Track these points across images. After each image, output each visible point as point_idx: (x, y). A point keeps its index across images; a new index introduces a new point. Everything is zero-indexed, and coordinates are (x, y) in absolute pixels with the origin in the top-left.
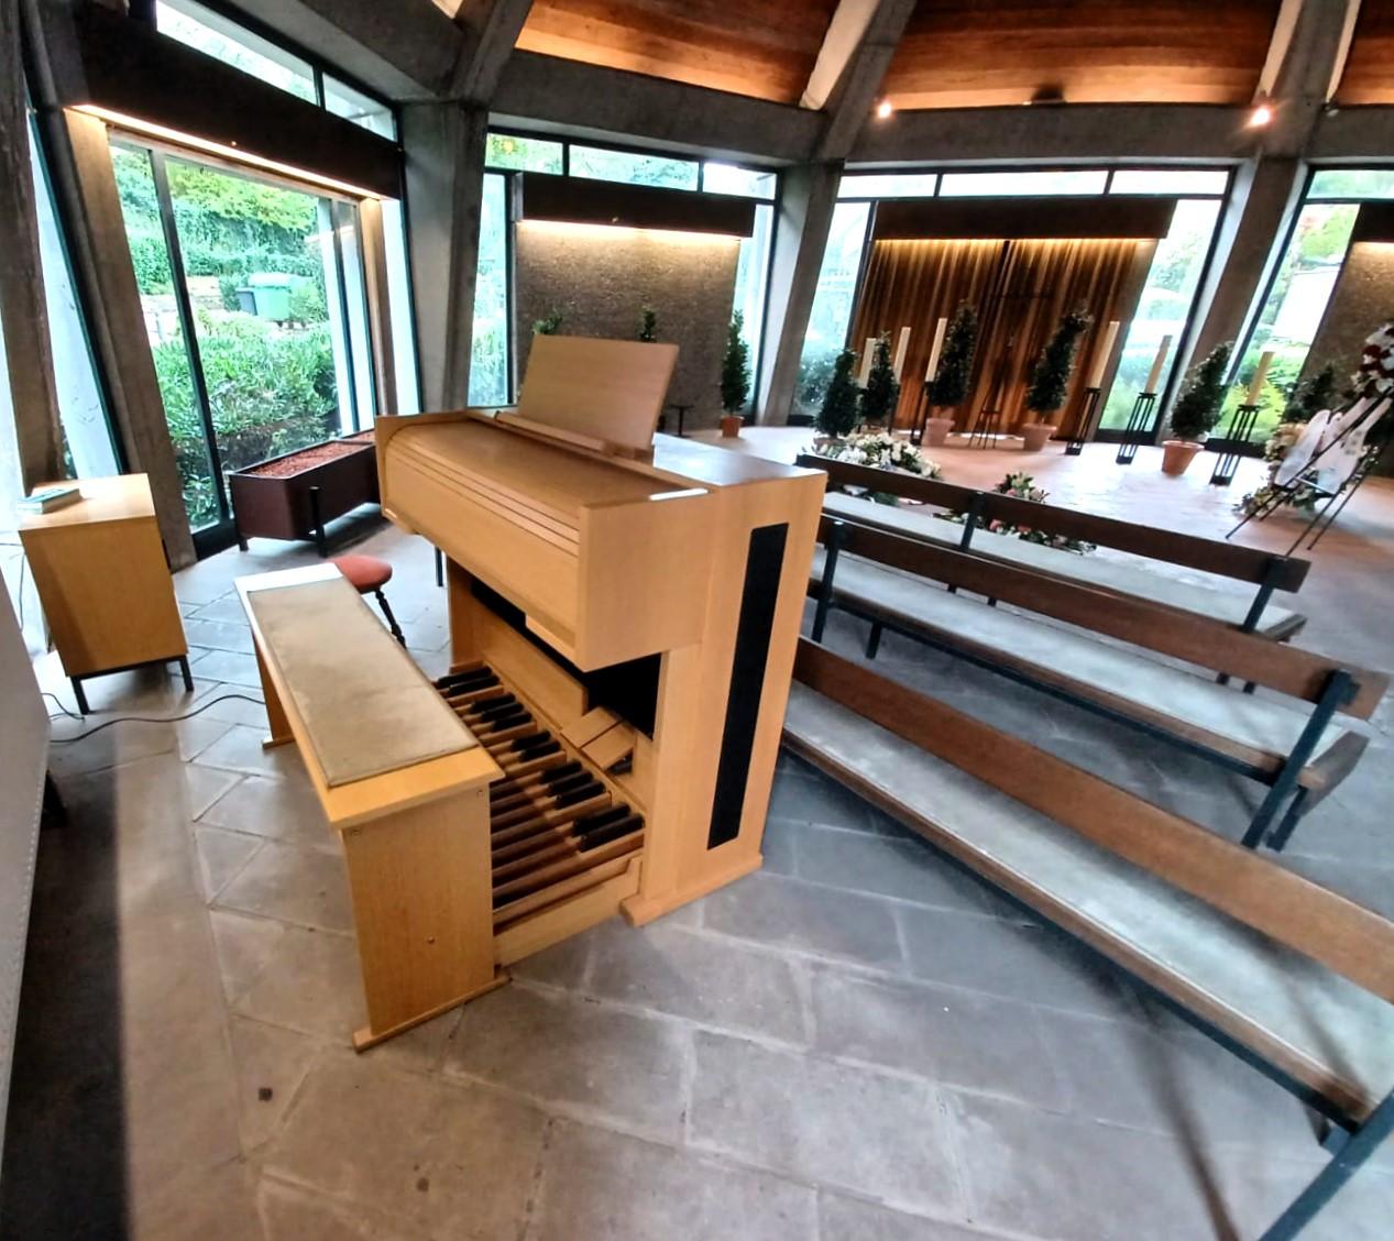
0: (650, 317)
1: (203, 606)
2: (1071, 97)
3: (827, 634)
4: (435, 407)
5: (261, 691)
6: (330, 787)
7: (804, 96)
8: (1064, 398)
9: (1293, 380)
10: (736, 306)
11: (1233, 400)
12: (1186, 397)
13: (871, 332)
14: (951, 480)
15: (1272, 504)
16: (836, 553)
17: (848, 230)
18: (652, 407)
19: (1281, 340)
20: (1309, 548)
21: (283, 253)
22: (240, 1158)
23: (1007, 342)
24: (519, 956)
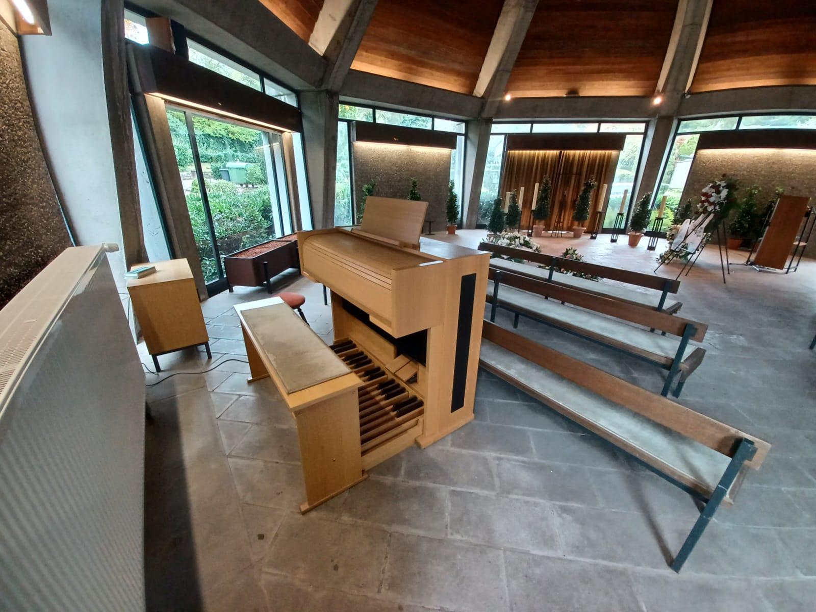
0: (414, 183)
1: (213, 319)
2: (582, 94)
3: (497, 319)
4: (319, 227)
5: (247, 357)
6: (289, 394)
7: (475, 91)
8: (588, 216)
9: (677, 206)
10: (451, 178)
11: (654, 215)
12: (635, 215)
13: (508, 190)
14: (544, 252)
15: (671, 257)
16: (498, 284)
17: (496, 146)
18: (419, 226)
19: (673, 190)
20: (686, 275)
21: (241, 152)
23: (563, 192)
24: (370, 467)
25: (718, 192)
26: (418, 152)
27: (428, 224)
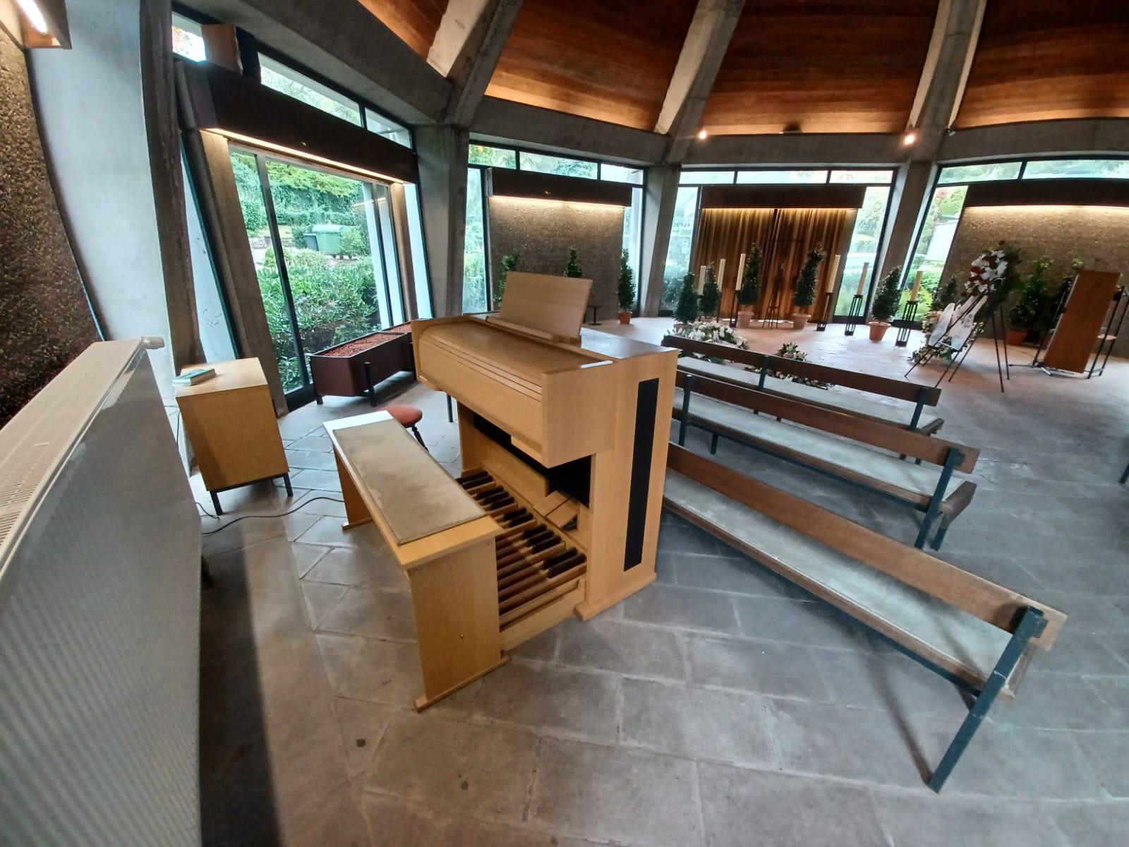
0: (573, 253)
1: (295, 441)
2: (805, 130)
3: (687, 441)
4: (441, 314)
5: (342, 494)
6: (400, 545)
7: (657, 127)
8: (813, 298)
10: (624, 247)
11: (905, 297)
12: (879, 297)
13: (703, 263)
14: (753, 349)
15: (928, 356)
16: (689, 393)
17: (686, 202)
18: (579, 313)
19: (931, 262)
20: (949, 381)
21: (334, 211)
22: (348, 783)
23: (779, 266)
24: (513, 646)
25: (994, 266)
26: (579, 211)
27: (593, 309)
